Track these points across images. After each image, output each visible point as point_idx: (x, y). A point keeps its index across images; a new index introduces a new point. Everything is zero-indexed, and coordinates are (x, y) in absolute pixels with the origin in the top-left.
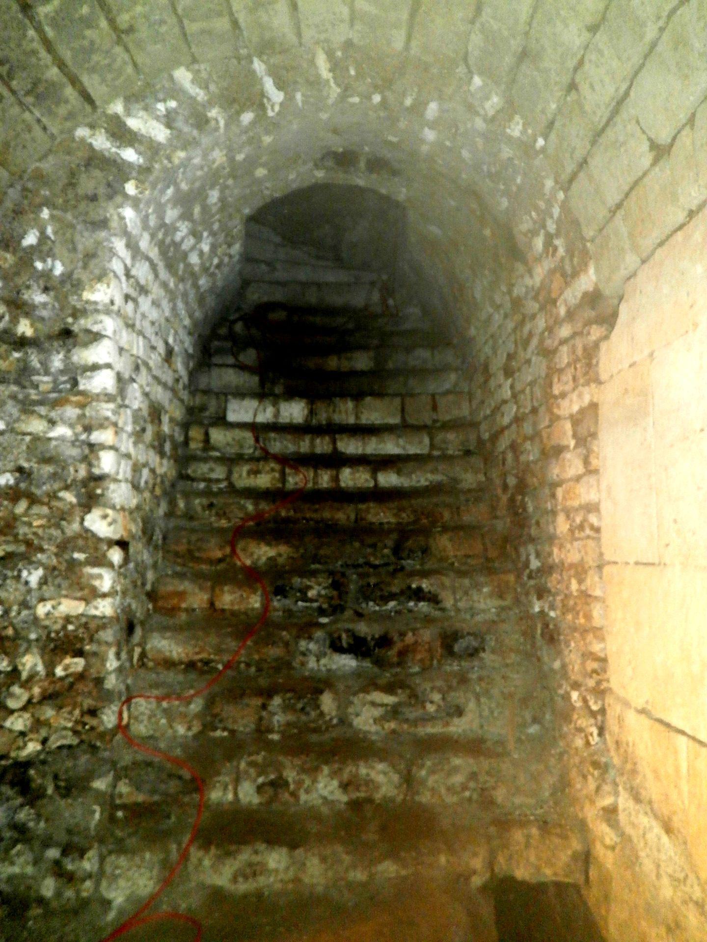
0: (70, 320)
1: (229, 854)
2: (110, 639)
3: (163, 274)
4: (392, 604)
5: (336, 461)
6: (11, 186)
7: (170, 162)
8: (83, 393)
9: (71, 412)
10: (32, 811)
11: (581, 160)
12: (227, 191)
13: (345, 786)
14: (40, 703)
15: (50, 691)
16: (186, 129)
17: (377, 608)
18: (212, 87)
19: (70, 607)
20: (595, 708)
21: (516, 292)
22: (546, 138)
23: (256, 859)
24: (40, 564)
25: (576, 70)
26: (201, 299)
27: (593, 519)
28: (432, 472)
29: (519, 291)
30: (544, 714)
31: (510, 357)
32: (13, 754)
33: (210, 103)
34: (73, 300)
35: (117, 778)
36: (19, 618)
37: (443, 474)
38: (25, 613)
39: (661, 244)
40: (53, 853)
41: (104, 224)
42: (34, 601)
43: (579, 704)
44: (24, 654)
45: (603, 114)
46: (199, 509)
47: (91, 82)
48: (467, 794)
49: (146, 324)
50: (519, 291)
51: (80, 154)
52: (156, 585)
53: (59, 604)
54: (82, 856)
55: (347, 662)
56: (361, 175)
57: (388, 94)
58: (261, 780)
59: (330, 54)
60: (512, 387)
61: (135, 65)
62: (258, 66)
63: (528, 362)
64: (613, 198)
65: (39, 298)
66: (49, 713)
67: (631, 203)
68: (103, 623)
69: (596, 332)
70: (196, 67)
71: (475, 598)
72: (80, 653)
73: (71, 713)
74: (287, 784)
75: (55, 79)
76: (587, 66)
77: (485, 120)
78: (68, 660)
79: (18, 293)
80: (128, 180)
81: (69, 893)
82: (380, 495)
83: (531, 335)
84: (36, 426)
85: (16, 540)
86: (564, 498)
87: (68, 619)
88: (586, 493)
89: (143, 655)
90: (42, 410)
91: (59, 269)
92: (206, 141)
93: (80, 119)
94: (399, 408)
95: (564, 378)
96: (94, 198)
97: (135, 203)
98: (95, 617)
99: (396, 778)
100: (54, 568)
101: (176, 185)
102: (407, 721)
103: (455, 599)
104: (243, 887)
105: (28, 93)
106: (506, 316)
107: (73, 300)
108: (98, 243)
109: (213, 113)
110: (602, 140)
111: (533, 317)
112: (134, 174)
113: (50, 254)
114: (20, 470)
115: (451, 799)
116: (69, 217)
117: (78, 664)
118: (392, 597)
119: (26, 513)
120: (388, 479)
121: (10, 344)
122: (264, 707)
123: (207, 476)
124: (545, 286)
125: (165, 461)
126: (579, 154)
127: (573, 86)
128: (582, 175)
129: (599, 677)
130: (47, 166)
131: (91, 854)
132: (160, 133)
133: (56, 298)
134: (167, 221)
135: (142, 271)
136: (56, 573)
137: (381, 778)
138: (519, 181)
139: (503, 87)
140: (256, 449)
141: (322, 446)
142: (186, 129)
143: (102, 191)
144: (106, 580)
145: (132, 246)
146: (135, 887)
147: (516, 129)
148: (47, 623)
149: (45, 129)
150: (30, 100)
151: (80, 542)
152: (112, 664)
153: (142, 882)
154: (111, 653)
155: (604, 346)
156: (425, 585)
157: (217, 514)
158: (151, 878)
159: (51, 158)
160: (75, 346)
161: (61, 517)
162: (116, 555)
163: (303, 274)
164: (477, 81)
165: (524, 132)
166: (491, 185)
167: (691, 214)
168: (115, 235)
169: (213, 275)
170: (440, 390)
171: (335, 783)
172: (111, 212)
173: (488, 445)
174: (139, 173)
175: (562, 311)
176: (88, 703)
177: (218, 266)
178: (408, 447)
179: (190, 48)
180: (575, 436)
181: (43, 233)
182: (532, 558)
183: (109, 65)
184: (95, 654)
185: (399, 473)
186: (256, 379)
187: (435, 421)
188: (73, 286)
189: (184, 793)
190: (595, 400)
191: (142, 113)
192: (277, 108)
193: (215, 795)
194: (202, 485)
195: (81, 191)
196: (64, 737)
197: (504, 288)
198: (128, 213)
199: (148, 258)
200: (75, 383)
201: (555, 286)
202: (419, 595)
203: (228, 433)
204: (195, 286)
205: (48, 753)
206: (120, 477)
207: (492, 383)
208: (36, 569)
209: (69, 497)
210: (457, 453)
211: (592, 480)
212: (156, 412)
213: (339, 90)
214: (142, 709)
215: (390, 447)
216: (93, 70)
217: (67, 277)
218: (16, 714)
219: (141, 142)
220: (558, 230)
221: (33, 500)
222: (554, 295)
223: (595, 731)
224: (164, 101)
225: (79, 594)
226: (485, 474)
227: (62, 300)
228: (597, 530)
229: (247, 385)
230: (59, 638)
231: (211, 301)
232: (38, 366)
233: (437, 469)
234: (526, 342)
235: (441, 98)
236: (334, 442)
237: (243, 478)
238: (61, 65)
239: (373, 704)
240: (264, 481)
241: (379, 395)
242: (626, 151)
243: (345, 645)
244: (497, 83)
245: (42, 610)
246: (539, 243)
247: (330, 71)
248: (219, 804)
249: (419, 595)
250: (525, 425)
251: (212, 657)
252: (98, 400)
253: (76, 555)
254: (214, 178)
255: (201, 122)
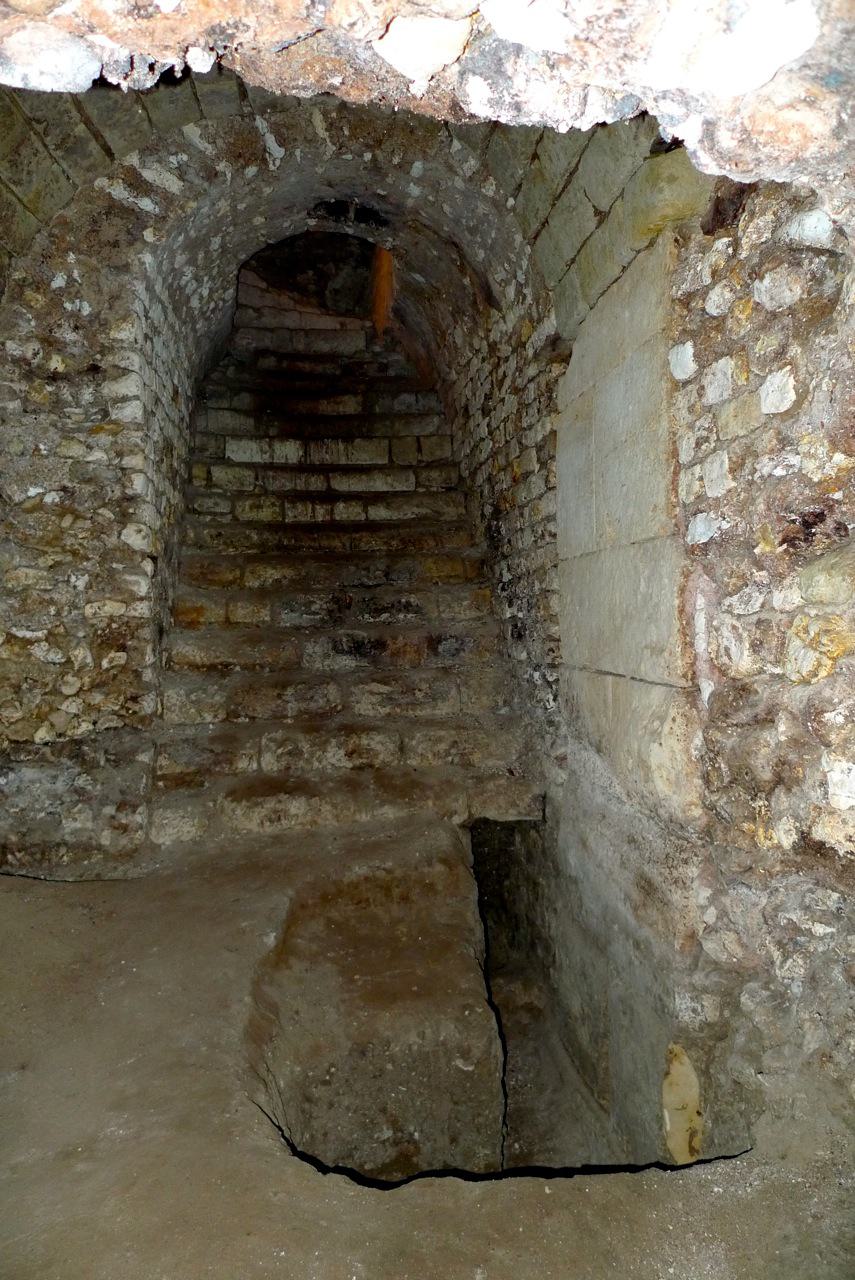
0: (98, 357)
1: (257, 804)
2: (148, 636)
3: (171, 317)
4: (385, 616)
5: (330, 497)
6: (39, 231)
7: (184, 212)
8: (115, 422)
9: (105, 439)
10: (89, 778)
11: (543, 220)
12: (228, 238)
13: (350, 755)
14: (90, 690)
15: (98, 681)
16: (197, 181)
17: (372, 620)
18: (220, 142)
19: (113, 608)
20: (551, 679)
21: (493, 336)
22: (515, 198)
23: (279, 807)
24: (85, 571)
25: (538, 143)
26: (197, 343)
27: (551, 527)
28: (418, 506)
29: (494, 336)
30: (513, 698)
31: (488, 397)
32: (69, 733)
33: (218, 158)
34: (102, 338)
35: (158, 754)
36: (70, 617)
37: (428, 508)
38: (74, 612)
39: (602, 294)
40: (109, 810)
41: (125, 268)
42: (82, 603)
43: (539, 682)
44: (75, 648)
45: (559, 183)
46: (209, 539)
47: (112, 137)
48: (450, 758)
49: (159, 363)
50: (494, 336)
51: (100, 202)
52: (176, 602)
53: (104, 605)
54: (134, 812)
55: (347, 662)
56: (351, 224)
57: (378, 152)
58: (280, 751)
59: (325, 114)
60: (488, 425)
61: (150, 120)
62: (260, 123)
63: (503, 400)
64: (569, 254)
65: (70, 336)
66: (97, 698)
67: (582, 258)
68: (141, 623)
69: (556, 369)
70: (204, 122)
71: (457, 610)
72: (123, 648)
73: (117, 699)
74: (301, 753)
75: (83, 135)
76: (545, 140)
77: (464, 181)
78: (112, 654)
79: (50, 331)
80: (146, 227)
81: (124, 841)
82: (372, 527)
83: (505, 375)
84: (76, 450)
85: (64, 551)
86: (530, 515)
87: (112, 619)
88: (546, 507)
89: (169, 660)
90: (81, 437)
91: (86, 310)
92: (214, 192)
93: (100, 169)
94: (387, 449)
95: (531, 411)
96: (116, 244)
97: (154, 249)
98: (134, 617)
99: (391, 747)
100: (98, 575)
101: (187, 232)
102: (399, 705)
103: (439, 612)
104: (269, 829)
105: (58, 147)
106: (484, 360)
107: (102, 338)
108: (122, 286)
109: (221, 166)
110: (558, 204)
111: (507, 359)
112: (151, 222)
113: (78, 295)
114: (64, 489)
115: (435, 763)
116: (94, 261)
117: (121, 657)
118: (385, 610)
119: (71, 527)
120: (379, 513)
121: (45, 378)
122: (279, 696)
123: (212, 510)
124: (516, 332)
125: (176, 493)
126: (542, 215)
127: (535, 156)
128: (544, 232)
129: (555, 654)
130: (71, 213)
131: (140, 809)
132: (174, 185)
133: (85, 337)
134: (176, 266)
135: (156, 313)
136: (100, 579)
137: (379, 747)
138: (493, 236)
139: (479, 151)
140: (256, 486)
141: (316, 483)
142: (197, 181)
143: (123, 237)
144: (143, 587)
145: (149, 289)
146: (180, 834)
147: (490, 189)
148: (94, 621)
149: (68, 178)
150: (59, 153)
151: (118, 554)
152: (149, 659)
153: (186, 828)
154: (149, 649)
155: (561, 381)
156: (413, 599)
157: (225, 543)
158: (194, 825)
159: (73, 206)
160: (104, 380)
161: (98, 531)
162: (148, 566)
163: (291, 320)
164: (456, 145)
165: (497, 192)
166: (469, 237)
167: (624, 269)
168: (136, 278)
169: (207, 319)
170: (426, 432)
171: (342, 752)
172: (131, 257)
173: (468, 481)
174: (156, 222)
175: (530, 352)
176: (131, 691)
177: (213, 311)
178: (395, 484)
179: (199, 105)
180: (538, 460)
181: (70, 276)
182: (505, 572)
183: (128, 121)
184: (135, 649)
185: (388, 506)
186: (251, 422)
187: (420, 461)
188: (101, 325)
189: (216, 763)
190: (555, 428)
191: (156, 165)
192: (278, 163)
193: (242, 764)
194: (208, 518)
195: (104, 239)
196: (112, 721)
197: (482, 334)
198: (148, 258)
199: (161, 302)
200: (106, 414)
201: (525, 331)
202: (408, 607)
203: (229, 471)
204: (194, 330)
205: (97, 733)
206: (148, 499)
207: (472, 424)
208: (83, 575)
209: (107, 513)
210: (440, 490)
211: (550, 495)
212: (168, 448)
213: (334, 148)
214: (173, 701)
215: (380, 484)
216: (114, 126)
217: (95, 317)
218: (70, 699)
219: (157, 194)
220: (526, 280)
221: (77, 517)
222: (523, 339)
223: (551, 697)
224: (176, 154)
225: (120, 598)
226: (466, 507)
227: (91, 337)
228: (554, 536)
229: (243, 427)
230: (105, 635)
231: (206, 346)
232: (70, 398)
233: (422, 504)
234: (501, 383)
235: (425, 159)
236: (328, 480)
237: (245, 510)
238: (87, 122)
239: (372, 693)
240: (266, 514)
241: (368, 437)
242: (577, 214)
243: (345, 648)
244: (474, 149)
245: (89, 610)
246: (511, 291)
247: (326, 130)
248: (244, 772)
249: (408, 607)
250: (499, 457)
251: (231, 660)
252: (128, 429)
253: (114, 565)
254: (217, 227)
255: (212, 175)
